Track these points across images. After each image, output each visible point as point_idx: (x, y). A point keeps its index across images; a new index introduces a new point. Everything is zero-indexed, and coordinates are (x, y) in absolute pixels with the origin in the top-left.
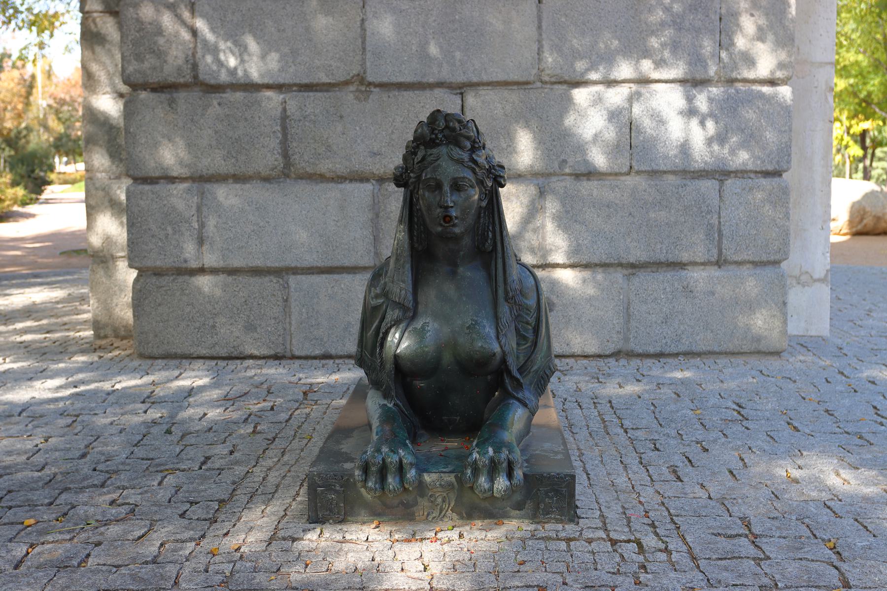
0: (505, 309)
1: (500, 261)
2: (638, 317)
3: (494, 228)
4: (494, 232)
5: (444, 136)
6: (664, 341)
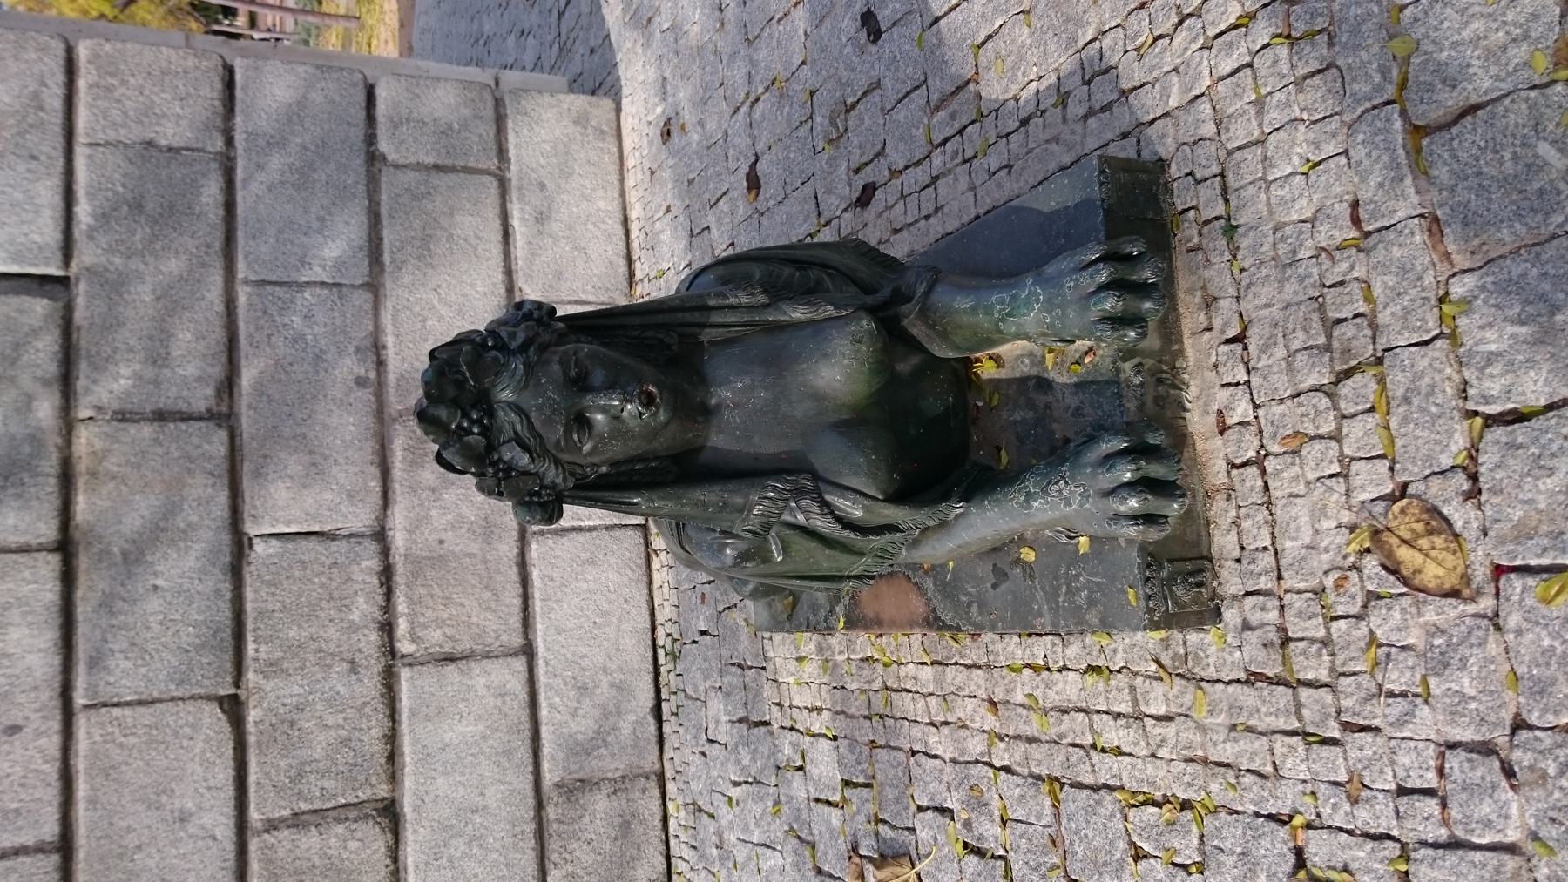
4: (645, 327)
5: (474, 406)
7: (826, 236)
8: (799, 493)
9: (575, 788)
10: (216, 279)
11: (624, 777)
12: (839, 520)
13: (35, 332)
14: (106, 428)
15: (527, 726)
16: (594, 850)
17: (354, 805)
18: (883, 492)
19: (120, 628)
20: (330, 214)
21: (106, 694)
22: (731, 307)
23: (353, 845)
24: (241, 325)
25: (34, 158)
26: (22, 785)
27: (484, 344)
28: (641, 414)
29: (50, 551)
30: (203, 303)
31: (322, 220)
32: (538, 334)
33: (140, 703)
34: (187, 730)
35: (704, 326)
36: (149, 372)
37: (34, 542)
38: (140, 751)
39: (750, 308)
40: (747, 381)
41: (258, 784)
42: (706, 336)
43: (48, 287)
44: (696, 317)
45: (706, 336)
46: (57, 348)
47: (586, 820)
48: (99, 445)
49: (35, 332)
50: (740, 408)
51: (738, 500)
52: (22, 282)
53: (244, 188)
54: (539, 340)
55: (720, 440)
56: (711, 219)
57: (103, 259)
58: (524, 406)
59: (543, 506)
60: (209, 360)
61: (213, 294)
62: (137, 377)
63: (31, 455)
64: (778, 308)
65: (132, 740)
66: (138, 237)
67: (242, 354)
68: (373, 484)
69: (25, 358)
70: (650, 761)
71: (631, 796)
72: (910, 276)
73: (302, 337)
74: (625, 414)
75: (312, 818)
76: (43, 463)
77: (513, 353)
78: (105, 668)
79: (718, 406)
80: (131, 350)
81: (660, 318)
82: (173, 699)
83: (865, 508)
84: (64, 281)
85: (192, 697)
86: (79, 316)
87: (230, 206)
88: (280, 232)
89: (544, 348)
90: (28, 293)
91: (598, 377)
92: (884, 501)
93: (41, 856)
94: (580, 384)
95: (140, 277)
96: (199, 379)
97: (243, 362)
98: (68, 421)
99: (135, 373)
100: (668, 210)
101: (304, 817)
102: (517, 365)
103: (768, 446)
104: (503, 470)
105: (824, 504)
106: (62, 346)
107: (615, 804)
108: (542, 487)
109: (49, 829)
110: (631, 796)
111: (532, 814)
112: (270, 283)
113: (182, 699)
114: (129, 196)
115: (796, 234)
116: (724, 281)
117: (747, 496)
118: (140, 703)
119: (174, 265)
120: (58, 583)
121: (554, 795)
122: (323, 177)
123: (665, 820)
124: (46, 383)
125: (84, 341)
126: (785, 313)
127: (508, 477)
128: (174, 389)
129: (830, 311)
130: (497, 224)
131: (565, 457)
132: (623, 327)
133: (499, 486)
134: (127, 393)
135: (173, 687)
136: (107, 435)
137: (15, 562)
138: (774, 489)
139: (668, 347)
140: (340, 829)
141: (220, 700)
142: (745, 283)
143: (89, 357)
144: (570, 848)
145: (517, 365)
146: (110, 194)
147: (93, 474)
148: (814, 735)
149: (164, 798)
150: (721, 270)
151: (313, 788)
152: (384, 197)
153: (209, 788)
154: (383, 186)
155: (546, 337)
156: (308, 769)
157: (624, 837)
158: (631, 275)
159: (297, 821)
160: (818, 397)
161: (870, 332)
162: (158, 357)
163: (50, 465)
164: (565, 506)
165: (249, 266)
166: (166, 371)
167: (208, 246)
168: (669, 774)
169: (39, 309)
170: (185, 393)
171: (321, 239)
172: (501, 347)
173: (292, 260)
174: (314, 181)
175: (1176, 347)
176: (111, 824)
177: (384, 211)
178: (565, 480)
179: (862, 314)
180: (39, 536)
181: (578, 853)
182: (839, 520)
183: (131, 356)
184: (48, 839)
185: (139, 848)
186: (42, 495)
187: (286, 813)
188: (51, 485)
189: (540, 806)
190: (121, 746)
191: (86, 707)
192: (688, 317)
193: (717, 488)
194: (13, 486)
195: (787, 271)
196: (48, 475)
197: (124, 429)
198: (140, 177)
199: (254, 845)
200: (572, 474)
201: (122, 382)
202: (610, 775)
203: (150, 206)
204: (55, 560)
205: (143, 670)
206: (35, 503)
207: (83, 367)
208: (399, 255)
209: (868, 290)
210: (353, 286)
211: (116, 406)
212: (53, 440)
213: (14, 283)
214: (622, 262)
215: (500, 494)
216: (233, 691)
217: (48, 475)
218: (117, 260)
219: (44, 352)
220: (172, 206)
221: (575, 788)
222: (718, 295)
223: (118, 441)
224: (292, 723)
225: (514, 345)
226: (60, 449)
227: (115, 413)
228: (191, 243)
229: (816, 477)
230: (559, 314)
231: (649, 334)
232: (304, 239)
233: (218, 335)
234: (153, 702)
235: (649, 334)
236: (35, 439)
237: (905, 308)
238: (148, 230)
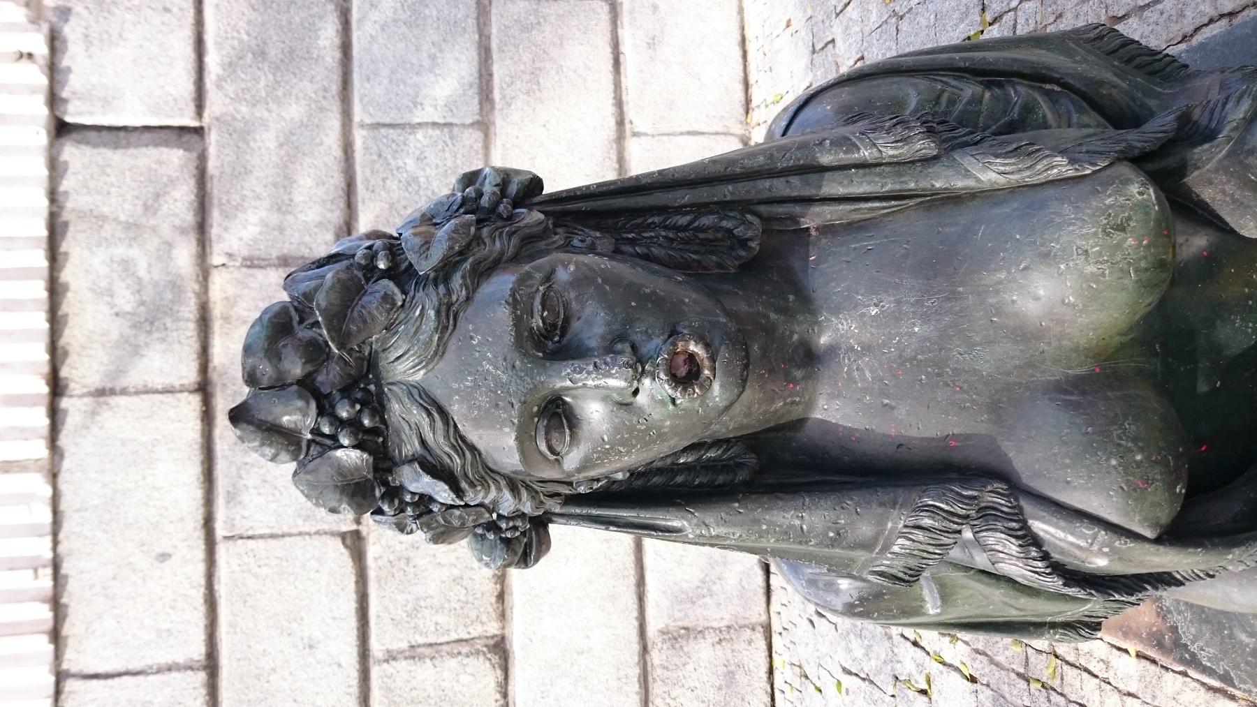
3: (680, 210)
4: (701, 208)
7: (994, 32)
8: (987, 515)
9: (680, 636)
10: (333, 122)
11: (729, 627)
12: (1058, 569)
13: (172, 182)
14: (237, 274)
15: (632, 572)
16: (697, 697)
17: (466, 641)
18: (1154, 525)
19: (253, 466)
20: (441, 51)
21: (241, 527)
22: (863, 166)
23: (465, 679)
24: (358, 169)
25: (167, 10)
26: (173, 608)
27: (369, 269)
29: (190, 392)
30: (321, 149)
31: (433, 58)
33: (272, 536)
34: (313, 563)
35: (808, 201)
36: (274, 219)
37: (177, 384)
38: (273, 581)
39: (898, 165)
40: (889, 303)
41: (378, 616)
42: (813, 218)
43: (186, 138)
44: (795, 186)
45: (813, 218)
46: (193, 197)
47: (690, 667)
48: (231, 290)
49: (172, 182)
50: (869, 362)
51: (865, 529)
52: (163, 134)
53: (359, 29)
55: (833, 412)
56: (837, 31)
57: (231, 108)
58: (438, 393)
60: (329, 205)
61: (332, 140)
62: (264, 224)
63: (172, 301)
64: (954, 164)
65: (265, 571)
66: (262, 84)
67: (360, 199)
69: (165, 208)
70: (757, 612)
71: (736, 647)
72: (1208, 88)
73: (416, 179)
74: (641, 399)
75: (428, 651)
76: (182, 308)
77: (422, 282)
78: (240, 503)
79: (833, 350)
80: (258, 198)
81: (727, 192)
82: (300, 534)
83: (1114, 553)
84: (199, 131)
85: (317, 533)
86: (212, 165)
87: (346, 48)
88: (393, 72)
89: (482, 273)
90: (166, 144)
91: (592, 322)
92: (1158, 541)
93: (189, 673)
94: (552, 342)
95: (265, 124)
96: (319, 225)
97: (360, 207)
98: (204, 271)
99: (262, 220)
100: (788, 25)
101: (420, 650)
102: (427, 304)
103: (916, 423)
105: (1030, 540)
106: (197, 196)
107: (720, 653)
109: (198, 650)
110: (736, 647)
111: (636, 659)
112: (384, 125)
113: (309, 534)
114: (253, 43)
115: (952, 36)
116: (851, 116)
117: (881, 522)
118: (272, 536)
119: (295, 111)
120: (199, 422)
121: (658, 640)
122: (434, 13)
123: (771, 671)
124: (183, 231)
125: (216, 189)
126: (967, 174)
128: (297, 235)
129: (1061, 167)
130: (607, 52)
132: (663, 210)
134: (255, 240)
135: (300, 522)
136: (238, 281)
137: (162, 402)
138: (933, 511)
139: (743, 243)
140: (453, 663)
141: (343, 536)
142: (892, 117)
143: (221, 205)
144: (673, 694)
145: (427, 304)
146: (236, 42)
147: (226, 319)
148: (943, 663)
149: (295, 626)
150: (845, 94)
151: (428, 623)
152: (494, 30)
153: (334, 618)
154: (494, 18)
156: (423, 604)
157: (728, 687)
158: (748, 101)
159: (413, 653)
160: (1024, 334)
161: (1144, 206)
162: (283, 207)
163: (189, 310)
165: (364, 109)
166: (290, 217)
167: (326, 90)
168: (776, 627)
169: (176, 160)
170: (307, 239)
171: (432, 78)
172: (401, 274)
173: (405, 101)
174: (425, 18)
176: (250, 647)
177: (494, 46)
179: (1125, 170)
180: (181, 378)
181: (681, 700)
182: (1058, 569)
183: (258, 203)
184: (196, 658)
185: (274, 670)
186: (182, 338)
187: (405, 645)
188: (190, 329)
189: (644, 650)
190: (256, 576)
191: (225, 538)
192: (780, 187)
193: (827, 502)
194: (158, 330)
195: (969, 90)
196: (188, 320)
197: (253, 275)
198: (263, 24)
199: (375, 672)
201: (250, 228)
202: (715, 624)
203: (273, 52)
204: (195, 400)
205: (273, 506)
206: (176, 347)
207: (215, 216)
208: (508, 92)
209: (1120, 118)
210: (463, 125)
211: (245, 252)
212: (193, 286)
213: (154, 135)
214: (739, 87)
216: (354, 527)
217: (188, 320)
218: (244, 109)
219: (181, 198)
220: (292, 51)
221: (680, 636)
222: (844, 143)
223: (248, 287)
224: (408, 560)
225: (424, 267)
226: (197, 295)
227: (244, 259)
228: (309, 88)
229: (1016, 488)
230: (548, 189)
231: (707, 221)
232: (415, 78)
233: (337, 180)
234: (283, 536)
235: (707, 221)
236: (175, 286)
237: (1200, 151)
238: (271, 77)
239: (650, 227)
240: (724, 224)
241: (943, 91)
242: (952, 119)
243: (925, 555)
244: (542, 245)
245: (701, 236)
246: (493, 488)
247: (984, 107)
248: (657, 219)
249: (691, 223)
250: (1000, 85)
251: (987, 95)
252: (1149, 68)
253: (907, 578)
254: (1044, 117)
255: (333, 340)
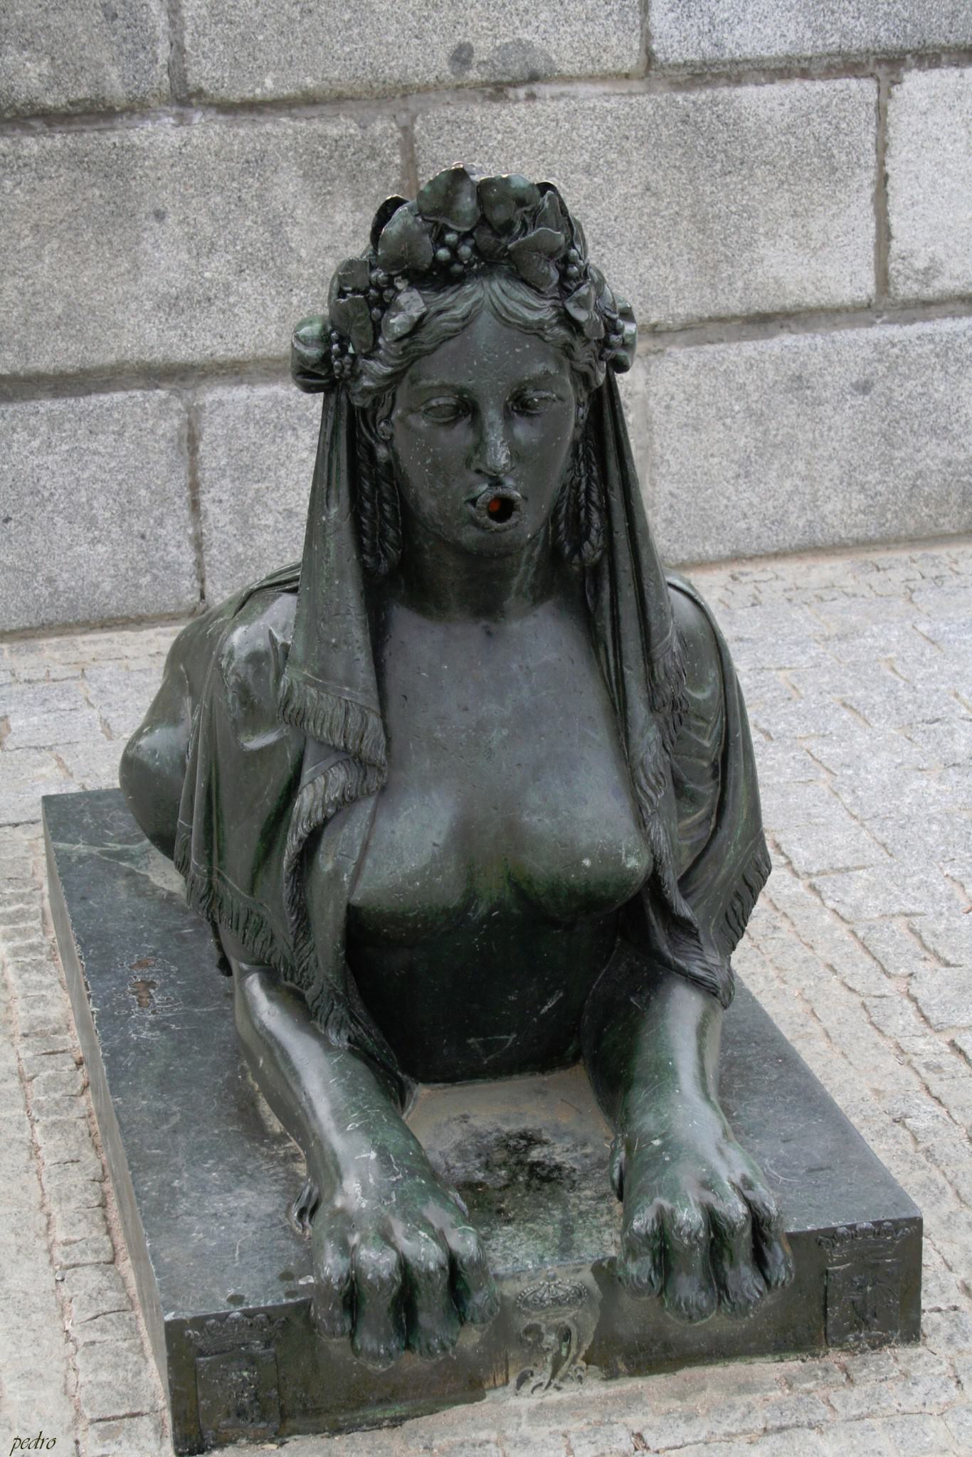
0: (647, 737)
1: (628, 608)
2: (674, 469)
3: (604, 493)
4: (607, 512)
5: (475, 249)
6: (742, 525)
28: (473, 502)
32: (588, 341)
54: (578, 344)
59: (319, 372)
68: (269, 83)
104: (381, 298)
108: (354, 357)
127: (371, 304)
131: (402, 392)
133: (355, 291)
155: (583, 355)
164: (321, 396)
175: (622, 1367)
178: (367, 391)
200: (376, 402)
215: (342, 294)
230: (618, 376)
231: (595, 517)
235: (595, 517)
239: (589, 469)
240: (594, 532)
241: (708, 722)
242: (682, 729)
243: (319, 722)
244: (581, 386)
245: (582, 514)
246: (398, 362)
247: (694, 760)
248: (595, 474)
249: (593, 504)
250: (714, 776)
251: (705, 764)
252: (731, 914)
253: (288, 711)
254: (689, 815)
255: (518, 245)
